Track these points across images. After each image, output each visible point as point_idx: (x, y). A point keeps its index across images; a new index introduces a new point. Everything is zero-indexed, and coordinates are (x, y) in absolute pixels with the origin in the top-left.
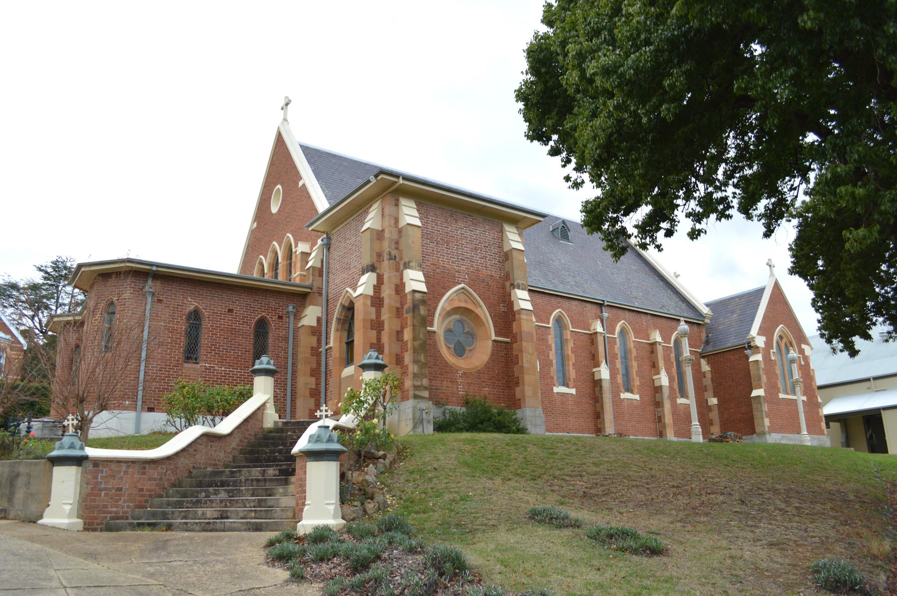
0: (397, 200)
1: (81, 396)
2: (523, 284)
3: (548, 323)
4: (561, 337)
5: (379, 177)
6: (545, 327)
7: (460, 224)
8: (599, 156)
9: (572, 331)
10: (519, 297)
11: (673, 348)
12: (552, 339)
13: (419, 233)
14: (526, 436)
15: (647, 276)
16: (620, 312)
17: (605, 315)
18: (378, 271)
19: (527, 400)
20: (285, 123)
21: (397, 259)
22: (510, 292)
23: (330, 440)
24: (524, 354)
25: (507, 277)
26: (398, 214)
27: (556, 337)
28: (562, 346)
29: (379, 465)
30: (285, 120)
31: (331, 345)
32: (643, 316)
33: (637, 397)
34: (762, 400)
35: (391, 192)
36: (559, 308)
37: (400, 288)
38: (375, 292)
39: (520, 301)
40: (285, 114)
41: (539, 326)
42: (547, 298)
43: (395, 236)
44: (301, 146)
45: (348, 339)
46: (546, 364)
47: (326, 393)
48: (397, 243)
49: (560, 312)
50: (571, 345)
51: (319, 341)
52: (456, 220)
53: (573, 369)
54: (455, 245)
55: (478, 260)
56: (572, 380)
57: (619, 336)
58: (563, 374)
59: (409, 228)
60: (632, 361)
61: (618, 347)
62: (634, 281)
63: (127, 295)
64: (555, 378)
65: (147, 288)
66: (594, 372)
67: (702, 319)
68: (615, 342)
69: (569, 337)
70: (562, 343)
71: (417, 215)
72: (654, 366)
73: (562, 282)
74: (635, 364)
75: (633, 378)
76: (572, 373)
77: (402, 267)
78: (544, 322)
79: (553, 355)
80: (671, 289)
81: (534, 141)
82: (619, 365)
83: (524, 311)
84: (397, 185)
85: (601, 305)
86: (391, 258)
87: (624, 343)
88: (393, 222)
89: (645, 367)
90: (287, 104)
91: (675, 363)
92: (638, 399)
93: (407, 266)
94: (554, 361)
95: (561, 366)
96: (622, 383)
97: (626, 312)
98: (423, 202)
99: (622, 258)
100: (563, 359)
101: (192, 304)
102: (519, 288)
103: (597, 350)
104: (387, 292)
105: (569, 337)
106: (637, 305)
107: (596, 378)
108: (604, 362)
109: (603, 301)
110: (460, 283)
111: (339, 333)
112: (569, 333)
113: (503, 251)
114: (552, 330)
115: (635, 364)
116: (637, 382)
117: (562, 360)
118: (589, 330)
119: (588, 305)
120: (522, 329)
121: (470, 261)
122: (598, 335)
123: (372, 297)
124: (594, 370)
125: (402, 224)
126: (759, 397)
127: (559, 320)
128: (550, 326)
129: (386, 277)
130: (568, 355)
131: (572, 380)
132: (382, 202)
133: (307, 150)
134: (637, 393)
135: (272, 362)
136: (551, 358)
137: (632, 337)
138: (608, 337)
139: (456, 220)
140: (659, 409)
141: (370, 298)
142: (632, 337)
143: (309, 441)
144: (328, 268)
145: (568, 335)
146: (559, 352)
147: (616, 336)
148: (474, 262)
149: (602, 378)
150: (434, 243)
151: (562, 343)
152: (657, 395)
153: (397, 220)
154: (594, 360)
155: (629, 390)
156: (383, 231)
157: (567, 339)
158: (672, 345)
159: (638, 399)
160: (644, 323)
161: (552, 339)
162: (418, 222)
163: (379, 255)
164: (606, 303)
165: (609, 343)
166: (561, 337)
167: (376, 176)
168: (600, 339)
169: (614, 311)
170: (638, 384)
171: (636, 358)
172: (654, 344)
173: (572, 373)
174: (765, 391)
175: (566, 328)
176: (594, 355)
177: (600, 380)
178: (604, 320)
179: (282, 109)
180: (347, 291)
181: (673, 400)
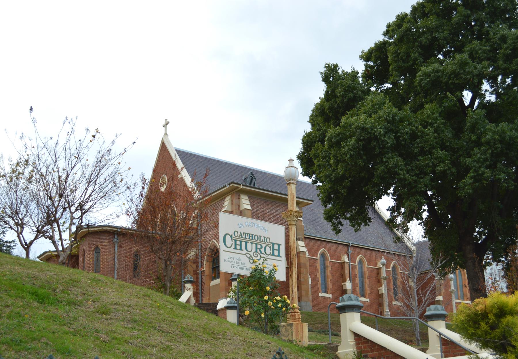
0: (239, 196)
2: (301, 238)
3: (317, 257)
4: (324, 265)
5: (231, 185)
6: (315, 259)
7: (270, 207)
8: (325, 200)
11: (391, 272)
12: (319, 266)
15: (379, 226)
16: (359, 250)
17: (350, 251)
19: (303, 297)
20: (166, 137)
23: (234, 303)
24: (302, 275)
26: (240, 203)
27: (321, 265)
28: (324, 270)
29: (244, 318)
30: (166, 134)
31: (204, 269)
32: (373, 252)
33: (368, 300)
34: (441, 302)
35: (236, 192)
36: (323, 247)
39: (300, 247)
40: (166, 130)
41: (311, 258)
42: (316, 242)
44: (176, 150)
45: (213, 266)
46: (315, 281)
47: (202, 294)
50: (329, 269)
51: (197, 267)
52: (268, 205)
56: (330, 289)
57: (358, 264)
58: (325, 286)
59: (246, 211)
60: (365, 279)
61: (357, 271)
62: (371, 230)
63: (105, 243)
64: (320, 288)
65: (115, 240)
67: (411, 253)
68: (356, 268)
69: (328, 265)
70: (325, 268)
71: (249, 203)
72: (379, 282)
73: (325, 232)
74: (367, 281)
75: (366, 289)
76: (330, 285)
78: (314, 256)
79: (319, 275)
80: (393, 234)
81: (320, 100)
82: (357, 281)
83: (302, 253)
84: (239, 189)
85: (347, 246)
87: (361, 268)
88: (237, 207)
89: (373, 282)
90: (167, 124)
91: (392, 280)
92: (369, 301)
94: (320, 279)
95: (324, 282)
96: (359, 292)
97: (363, 250)
98: (251, 196)
99: (339, 234)
100: (325, 277)
101: (135, 248)
103: (345, 272)
105: (328, 265)
106: (369, 245)
108: (348, 279)
109: (349, 243)
111: (208, 263)
112: (328, 262)
114: (319, 261)
115: (367, 281)
116: (368, 291)
117: (325, 278)
118: (341, 261)
119: (341, 246)
120: (301, 262)
122: (345, 263)
124: (343, 284)
125: (242, 209)
126: (439, 300)
127: (323, 255)
128: (318, 258)
130: (328, 275)
131: (330, 289)
132: (232, 196)
133: (178, 152)
134: (368, 298)
135: (192, 277)
136: (318, 276)
137: (366, 264)
139: (268, 205)
140: (381, 307)
142: (366, 264)
143: (227, 304)
145: (328, 264)
146: (323, 273)
147: (356, 264)
149: (347, 288)
151: (325, 268)
152: (380, 299)
153: (239, 206)
154: (343, 278)
155: (363, 296)
157: (327, 266)
158: (391, 269)
159: (369, 301)
160: (374, 256)
161: (319, 266)
162: (249, 207)
164: (351, 245)
165: (352, 268)
166: (324, 265)
167: (229, 184)
168: (347, 266)
169: (356, 249)
170: (369, 292)
171: (368, 277)
172: (379, 269)
173: (330, 285)
174: (443, 297)
175: (327, 259)
176: (343, 275)
178: (350, 255)
179: (164, 127)
180: (213, 241)
181: (390, 302)
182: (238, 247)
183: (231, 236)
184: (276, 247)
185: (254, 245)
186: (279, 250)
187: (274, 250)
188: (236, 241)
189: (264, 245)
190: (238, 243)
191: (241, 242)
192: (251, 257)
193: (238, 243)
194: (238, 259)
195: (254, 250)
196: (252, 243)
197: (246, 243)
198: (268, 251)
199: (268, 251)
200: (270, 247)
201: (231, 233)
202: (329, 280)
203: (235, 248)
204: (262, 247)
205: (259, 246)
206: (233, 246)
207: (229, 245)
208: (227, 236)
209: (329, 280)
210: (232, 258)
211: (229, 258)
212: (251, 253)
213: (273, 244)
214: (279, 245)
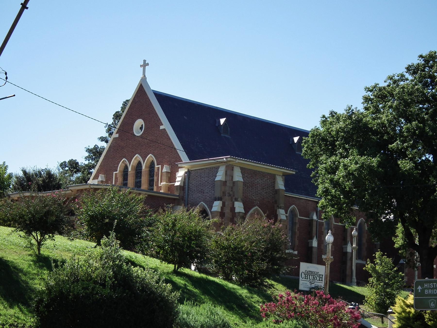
1: (265, 280)
9: (299, 218)
10: (281, 213)
13: (242, 184)
14: (62, 192)
18: (223, 200)
21: (232, 196)
22: (277, 210)
25: (276, 202)
37: (233, 209)
38: (221, 210)
43: (231, 185)
48: (232, 188)
49: (294, 206)
50: (298, 226)
53: (297, 240)
54: (255, 187)
55: (264, 194)
66: (309, 242)
69: (297, 221)
77: (234, 200)
84: (235, 162)
86: (230, 195)
88: (231, 178)
93: (236, 200)
102: (281, 209)
104: (227, 211)
107: (310, 246)
108: (315, 237)
110: (256, 206)
113: (275, 189)
121: (260, 195)
123: (220, 212)
129: (226, 203)
138: (319, 222)
141: (219, 213)
144: (188, 187)
148: (262, 195)
149: (313, 246)
150: (246, 187)
156: (226, 182)
163: (224, 193)
168: (315, 224)
175: (296, 216)
177: (312, 247)
178: (318, 212)
182: (306, 278)
183: (304, 273)
184: (321, 276)
185: (312, 276)
186: (322, 278)
187: (320, 278)
188: (306, 275)
189: (316, 276)
190: (306, 276)
191: (307, 275)
192: (311, 282)
193: (306, 276)
194: (306, 284)
195: (312, 279)
196: (312, 276)
197: (309, 275)
198: (318, 279)
199: (318, 279)
200: (319, 277)
201: (304, 272)
202: (296, 237)
203: (305, 279)
204: (315, 277)
205: (314, 277)
206: (305, 278)
207: (303, 277)
208: (303, 273)
209: (296, 237)
210: (304, 283)
211: (303, 283)
212: (311, 280)
213: (320, 275)
214: (322, 275)
